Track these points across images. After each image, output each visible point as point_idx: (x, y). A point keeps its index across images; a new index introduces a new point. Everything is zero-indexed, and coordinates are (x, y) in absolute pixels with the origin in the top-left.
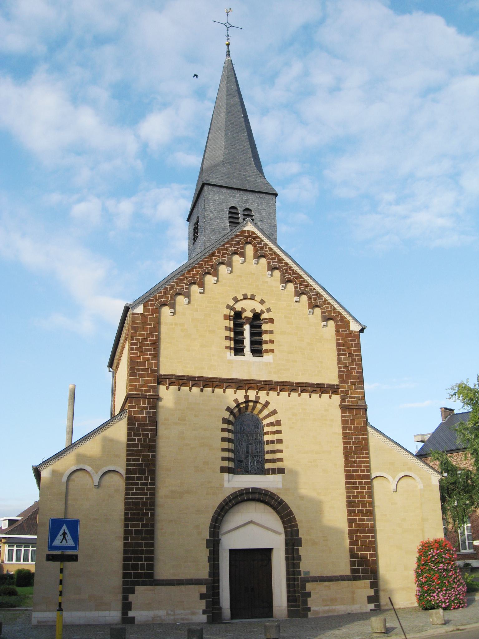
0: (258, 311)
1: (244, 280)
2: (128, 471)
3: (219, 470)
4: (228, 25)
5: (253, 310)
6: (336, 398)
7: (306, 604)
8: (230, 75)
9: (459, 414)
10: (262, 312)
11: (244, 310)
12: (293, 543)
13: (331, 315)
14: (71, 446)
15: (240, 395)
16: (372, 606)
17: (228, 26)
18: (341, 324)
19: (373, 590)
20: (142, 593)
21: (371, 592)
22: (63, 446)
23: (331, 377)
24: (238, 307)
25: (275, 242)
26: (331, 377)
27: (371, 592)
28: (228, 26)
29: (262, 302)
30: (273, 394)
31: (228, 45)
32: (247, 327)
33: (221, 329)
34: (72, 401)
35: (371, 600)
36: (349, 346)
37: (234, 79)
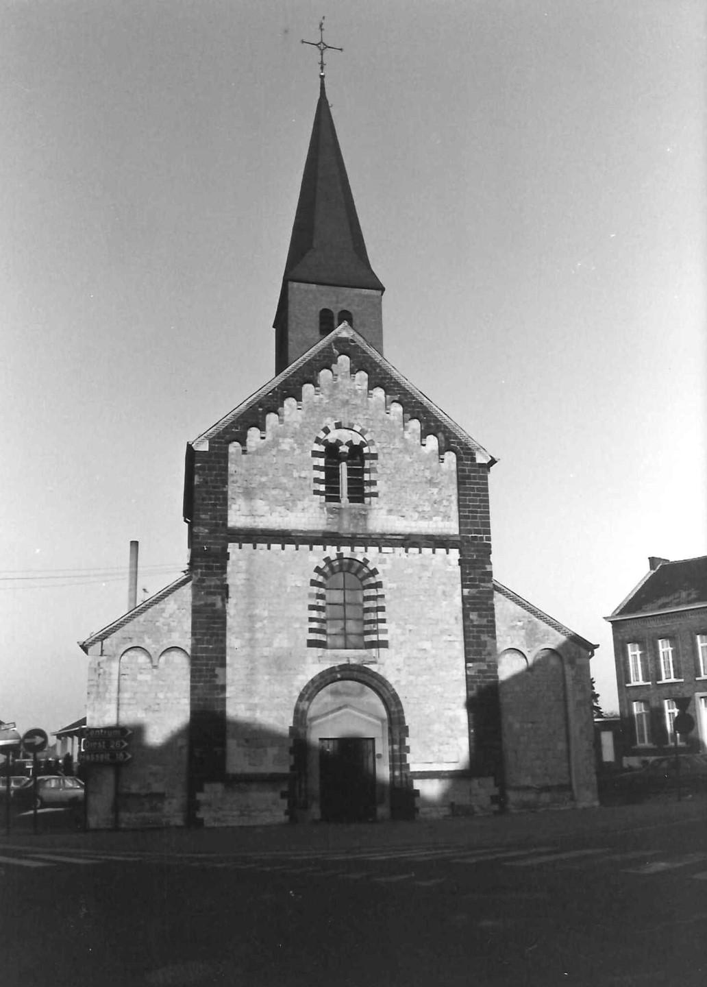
0: (356, 442)
1: (341, 404)
2: (193, 650)
3: (305, 643)
4: (322, 46)
5: (350, 444)
6: (455, 554)
7: (405, 761)
8: (323, 107)
9: (372, 289)
10: (363, 445)
11: (339, 443)
12: (397, 726)
13: (452, 442)
14: (136, 612)
15: (332, 551)
16: (496, 807)
17: (322, 47)
18: (465, 453)
19: (497, 789)
20: (211, 792)
21: (496, 791)
22: (123, 610)
23: (451, 527)
24: (333, 436)
25: (382, 355)
26: (451, 527)
27: (496, 791)
28: (322, 47)
29: (362, 433)
30: (373, 550)
31: (322, 77)
32: (344, 468)
33: (310, 470)
34: (134, 561)
35: (494, 799)
36: (472, 479)
37: (326, 741)
